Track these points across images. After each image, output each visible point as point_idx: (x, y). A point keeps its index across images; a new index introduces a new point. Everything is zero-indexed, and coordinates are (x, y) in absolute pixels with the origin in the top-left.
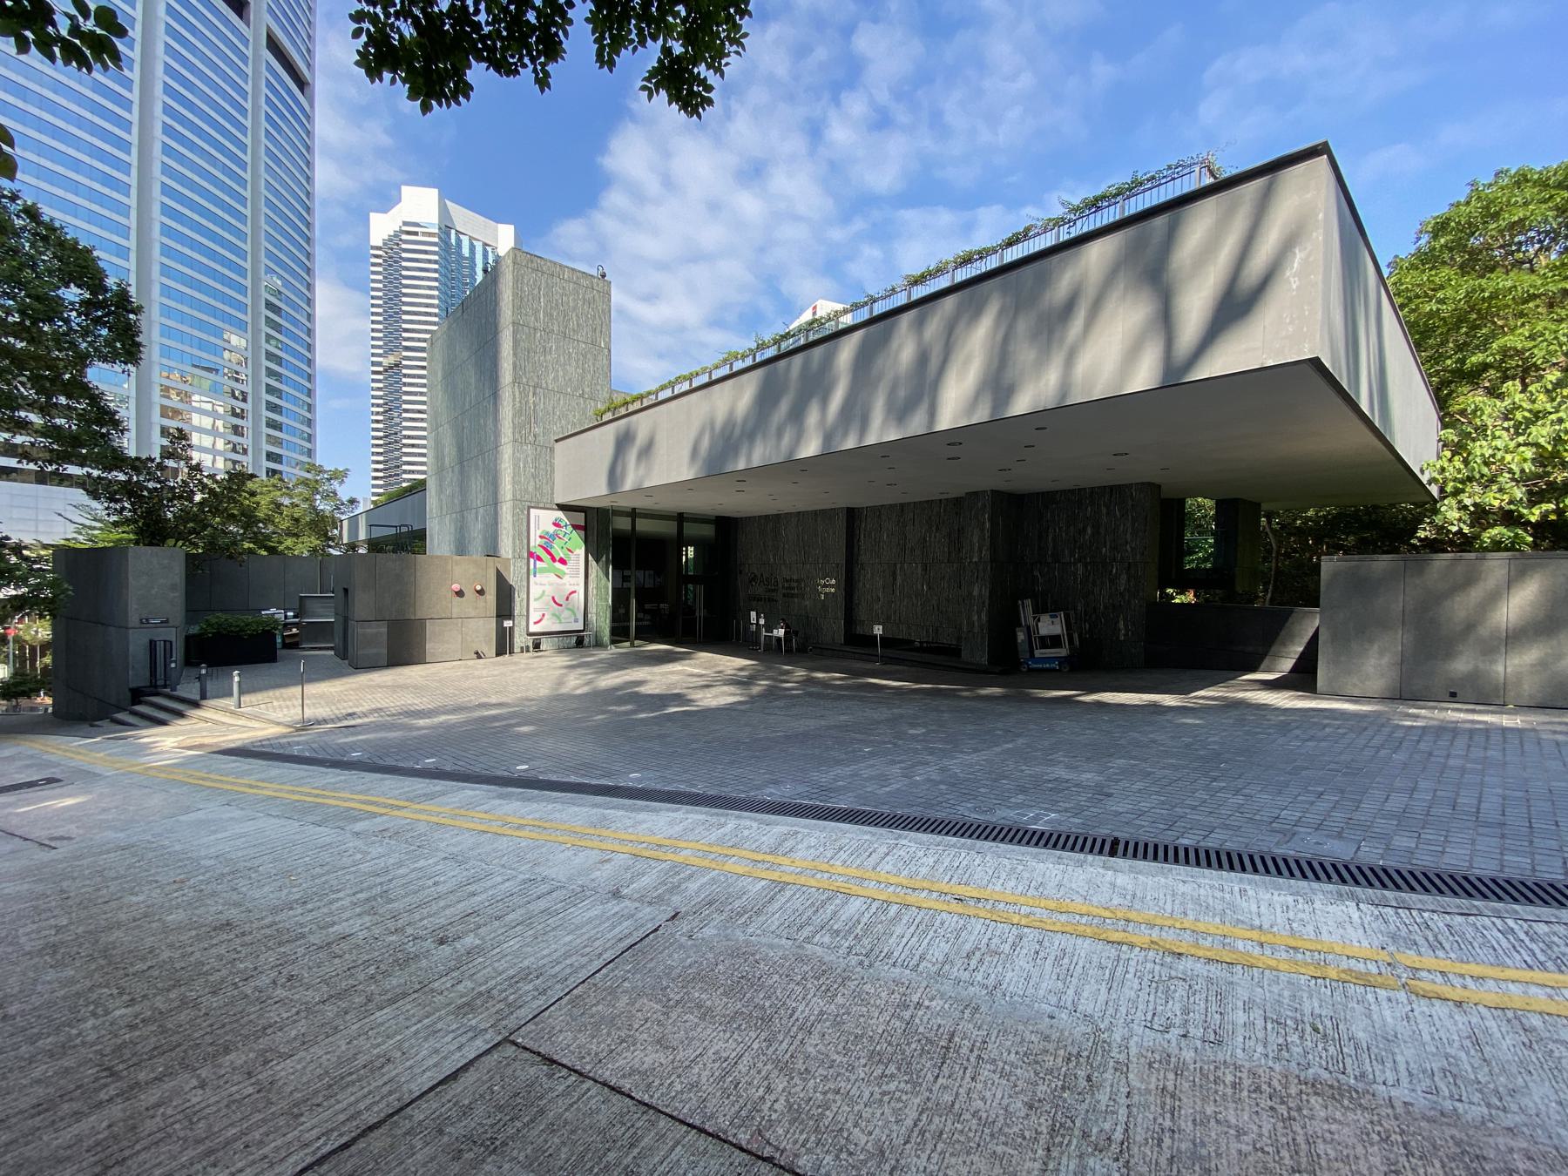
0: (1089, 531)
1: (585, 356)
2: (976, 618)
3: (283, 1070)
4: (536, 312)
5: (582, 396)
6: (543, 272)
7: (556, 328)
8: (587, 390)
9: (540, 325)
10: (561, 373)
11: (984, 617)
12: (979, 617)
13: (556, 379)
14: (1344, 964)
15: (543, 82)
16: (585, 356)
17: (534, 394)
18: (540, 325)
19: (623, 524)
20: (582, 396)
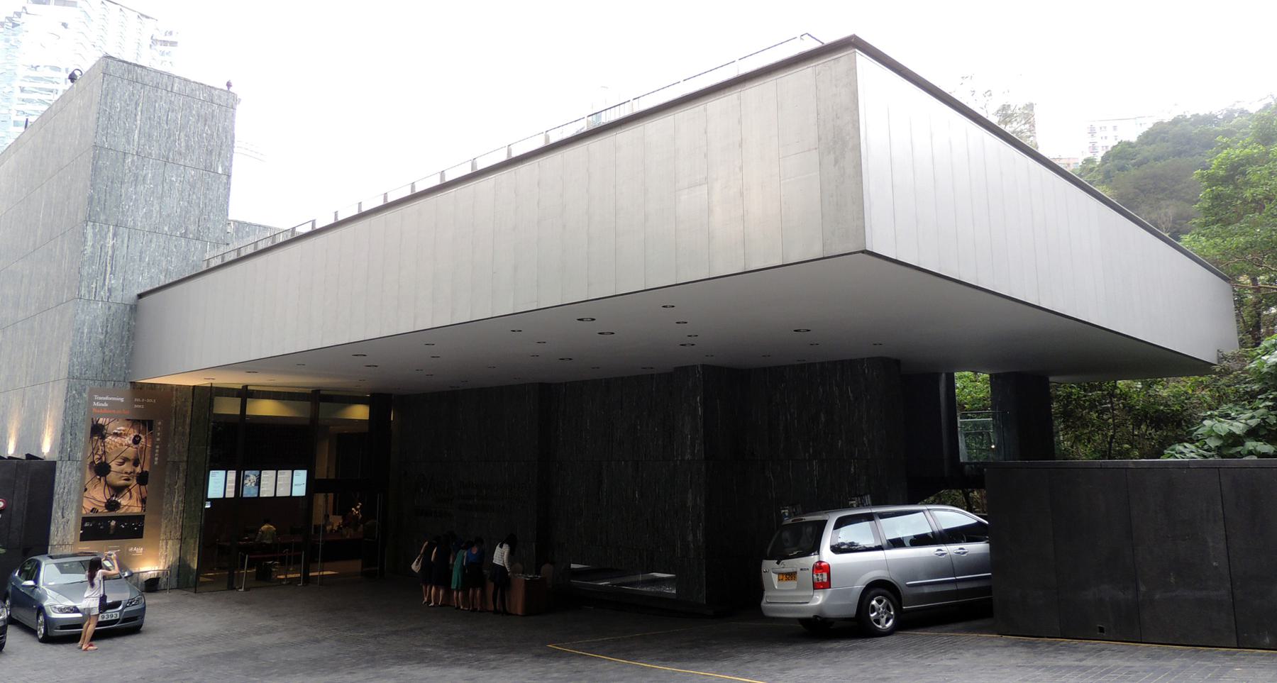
0: (823, 418)
1: (193, 186)
2: (690, 538)
3: (1243, 300)
4: (128, 133)
5: (184, 236)
6: (144, 85)
7: (155, 152)
8: (192, 228)
9: (132, 149)
10: (157, 207)
11: (700, 535)
12: (695, 535)
13: (148, 215)
14: (445, 663)
15: (336, 213)
16: (193, 186)
17: (115, 235)
18: (132, 149)
19: (229, 407)
20: (184, 236)
